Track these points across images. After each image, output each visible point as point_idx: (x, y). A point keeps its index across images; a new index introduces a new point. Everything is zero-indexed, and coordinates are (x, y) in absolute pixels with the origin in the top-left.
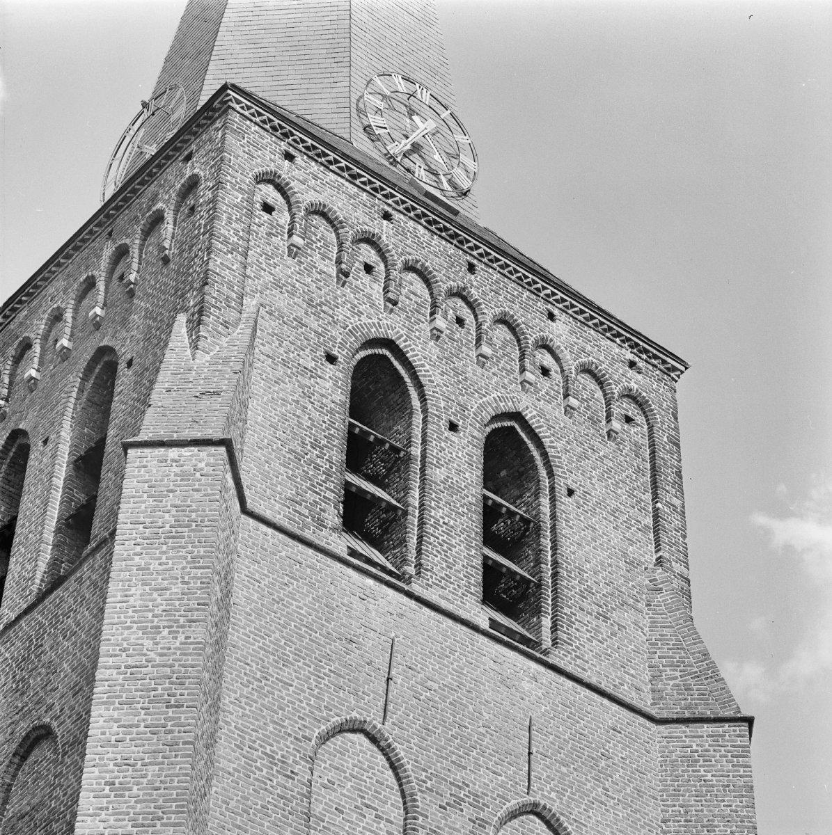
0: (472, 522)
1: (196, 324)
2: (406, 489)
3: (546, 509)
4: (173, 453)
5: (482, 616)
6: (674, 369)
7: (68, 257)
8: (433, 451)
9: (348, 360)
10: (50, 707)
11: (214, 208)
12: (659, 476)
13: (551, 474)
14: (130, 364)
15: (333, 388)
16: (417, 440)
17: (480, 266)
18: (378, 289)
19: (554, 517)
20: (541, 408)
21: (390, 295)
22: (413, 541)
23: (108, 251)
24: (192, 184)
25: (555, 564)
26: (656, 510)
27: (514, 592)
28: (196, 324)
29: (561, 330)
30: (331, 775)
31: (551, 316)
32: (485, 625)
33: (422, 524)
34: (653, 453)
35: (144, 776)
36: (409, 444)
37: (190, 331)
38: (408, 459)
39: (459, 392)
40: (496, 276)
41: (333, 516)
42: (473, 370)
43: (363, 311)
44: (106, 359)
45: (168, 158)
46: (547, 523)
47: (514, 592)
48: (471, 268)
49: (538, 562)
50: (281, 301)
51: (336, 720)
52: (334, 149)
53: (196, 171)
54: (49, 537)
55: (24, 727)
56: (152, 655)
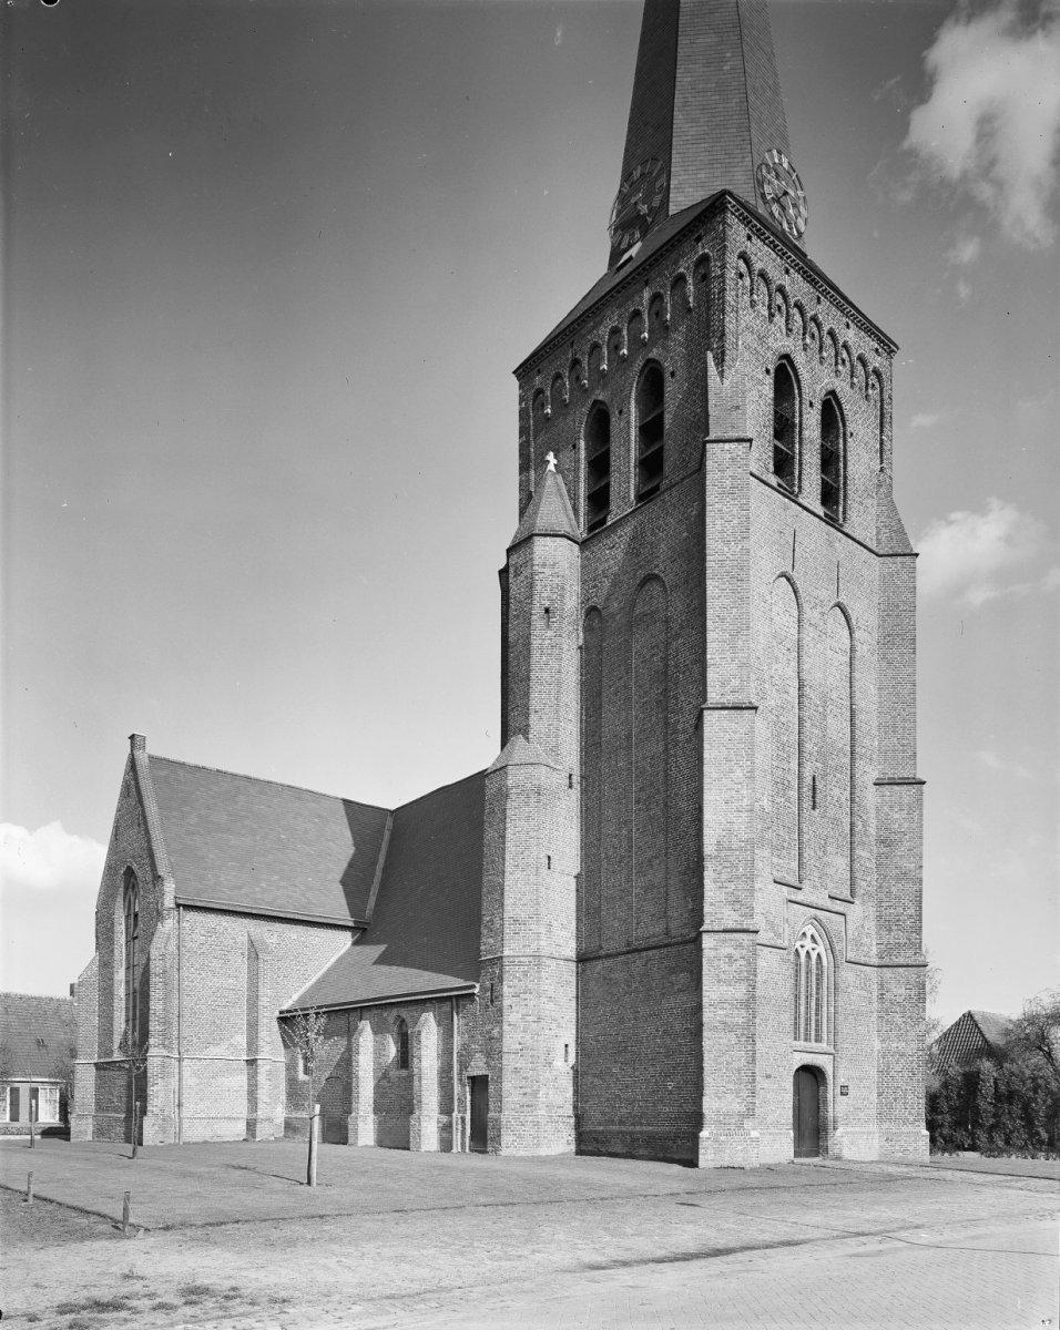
1: (720, 361)
2: (793, 443)
3: (841, 446)
4: (727, 446)
6: (893, 351)
7: (619, 292)
10: (657, 566)
11: (724, 282)
12: (883, 421)
13: (844, 425)
14: (673, 374)
16: (797, 414)
17: (754, 238)
18: (783, 320)
19: (845, 450)
20: (842, 387)
21: (790, 326)
22: (797, 473)
23: (647, 294)
24: (705, 259)
25: (845, 477)
26: (881, 440)
28: (720, 361)
29: (851, 335)
32: (822, 514)
33: (801, 464)
34: (882, 406)
36: (794, 417)
37: (717, 365)
38: (794, 425)
39: (815, 379)
42: (818, 366)
43: (782, 342)
44: (651, 365)
45: (685, 236)
46: (842, 453)
49: (838, 476)
52: (768, 229)
53: (706, 251)
54: (632, 469)
55: (641, 574)
56: (728, 555)
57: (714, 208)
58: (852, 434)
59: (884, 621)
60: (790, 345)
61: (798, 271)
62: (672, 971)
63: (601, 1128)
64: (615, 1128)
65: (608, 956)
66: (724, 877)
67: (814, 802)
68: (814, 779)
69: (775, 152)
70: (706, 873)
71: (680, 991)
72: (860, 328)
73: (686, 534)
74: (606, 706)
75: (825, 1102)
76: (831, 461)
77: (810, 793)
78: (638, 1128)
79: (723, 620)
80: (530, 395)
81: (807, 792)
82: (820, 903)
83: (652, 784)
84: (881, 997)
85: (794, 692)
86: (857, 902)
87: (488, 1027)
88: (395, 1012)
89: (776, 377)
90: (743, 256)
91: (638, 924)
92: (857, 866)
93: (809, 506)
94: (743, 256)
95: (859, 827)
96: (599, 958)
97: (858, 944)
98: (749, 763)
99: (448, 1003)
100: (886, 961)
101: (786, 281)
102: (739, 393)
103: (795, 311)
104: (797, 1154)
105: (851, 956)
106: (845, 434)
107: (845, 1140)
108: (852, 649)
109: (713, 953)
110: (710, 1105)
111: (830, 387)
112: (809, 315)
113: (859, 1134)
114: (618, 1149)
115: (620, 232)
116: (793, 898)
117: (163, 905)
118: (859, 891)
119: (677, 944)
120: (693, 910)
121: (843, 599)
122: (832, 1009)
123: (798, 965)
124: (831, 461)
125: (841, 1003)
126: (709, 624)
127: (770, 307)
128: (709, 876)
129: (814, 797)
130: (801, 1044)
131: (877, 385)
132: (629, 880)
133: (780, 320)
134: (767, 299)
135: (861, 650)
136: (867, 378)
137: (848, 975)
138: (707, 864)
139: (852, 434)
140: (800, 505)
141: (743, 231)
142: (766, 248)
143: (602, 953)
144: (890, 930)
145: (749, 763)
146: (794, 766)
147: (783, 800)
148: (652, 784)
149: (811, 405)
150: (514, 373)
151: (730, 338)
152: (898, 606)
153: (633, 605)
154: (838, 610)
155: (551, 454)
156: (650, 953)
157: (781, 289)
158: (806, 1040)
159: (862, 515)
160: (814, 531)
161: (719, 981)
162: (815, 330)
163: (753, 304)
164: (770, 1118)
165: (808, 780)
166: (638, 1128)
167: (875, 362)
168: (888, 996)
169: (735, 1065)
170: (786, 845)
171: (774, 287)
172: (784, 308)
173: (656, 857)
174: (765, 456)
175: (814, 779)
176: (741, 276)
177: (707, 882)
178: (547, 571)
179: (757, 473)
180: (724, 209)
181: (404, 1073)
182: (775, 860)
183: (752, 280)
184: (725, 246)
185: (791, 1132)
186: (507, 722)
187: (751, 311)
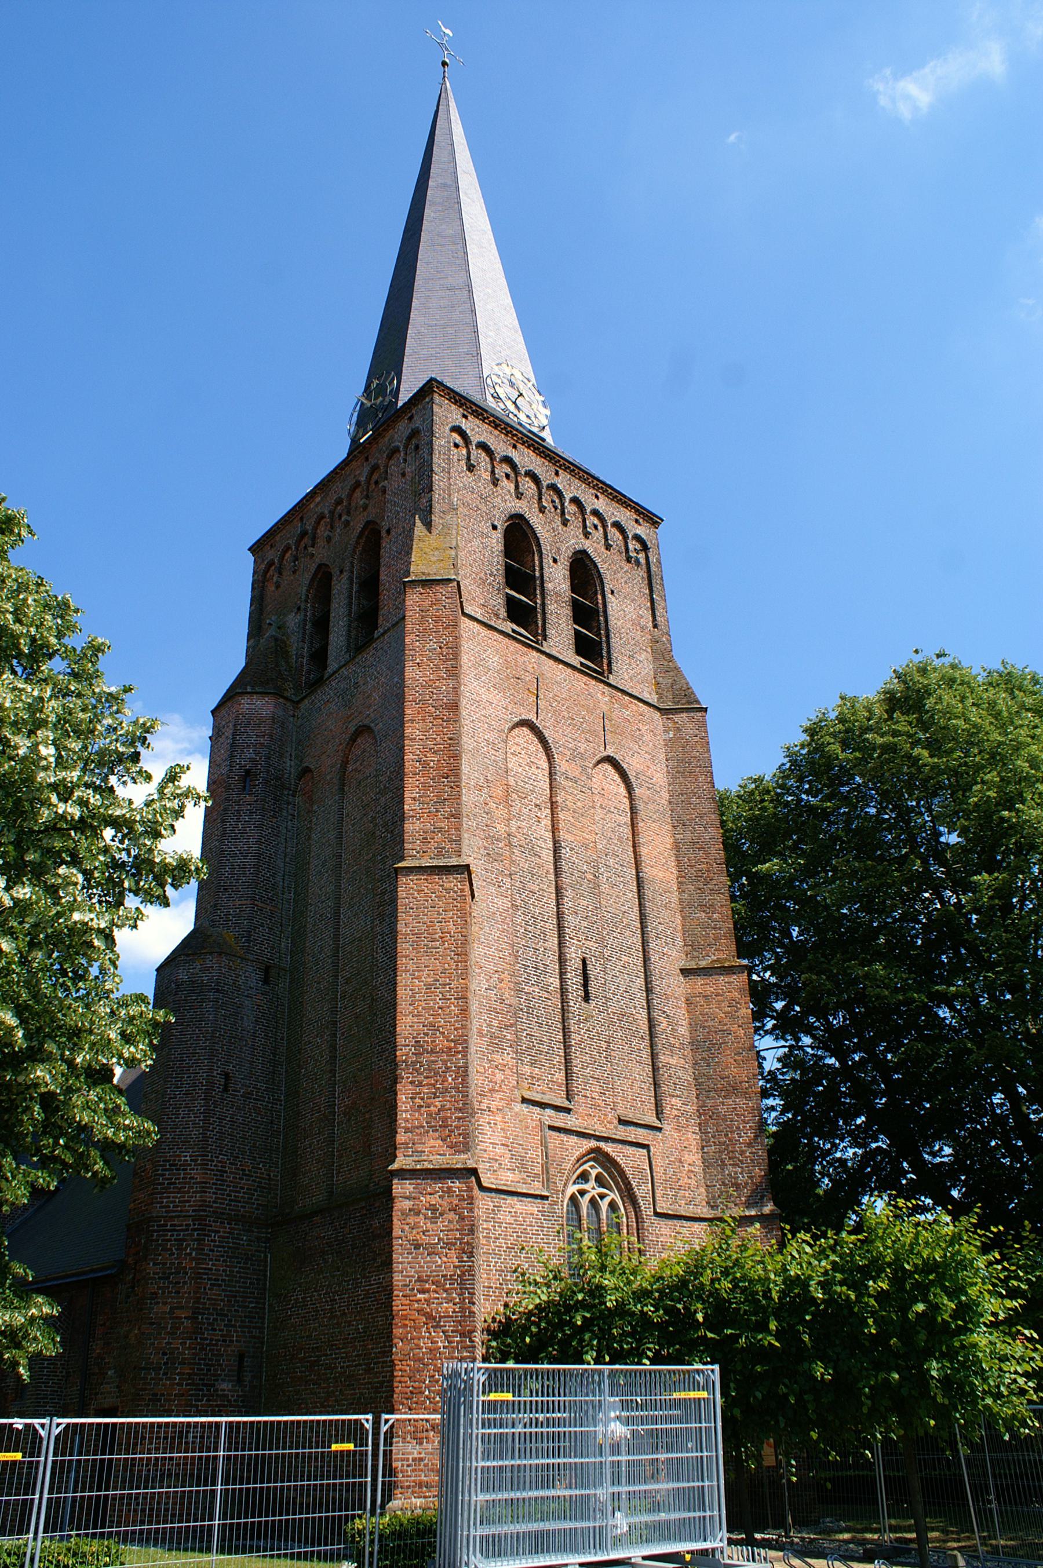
0: (567, 611)
5: (576, 660)
8: (546, 575)
9: (501, 526)
14: (388, 532)
15: (496, 541)
18: (513, 486)
20: (594, 547)
27: (593, 649)
29: (601, 504)
30: (515, 748)
31: (597, 497)
35: (426, 756)
36: (534, 571)
39: (557, 542)
40: (569, 476)
41: (503, 613)
43: (506, 502)
44: (371, 527)
47: (593, 649)
48: (557, 474)
49: (599, 629)
50: (468, 497)
51: (516, 720)
57: (429, 388)
61: (528, 447)
68: (584, 960)
77: (580, 979)
81: (574, 980)
82: (601, 1131)
85: (548, 856)
86: (665, 1126)
93: (557, 655)
95: (663, 1024)
134: (489, 466)
150: (249, 549)
154: (607, 767)
159: (633, 666)
160: (565, 682)
165: (574, 964)
175: (584, 960)
177: (402, 1098)
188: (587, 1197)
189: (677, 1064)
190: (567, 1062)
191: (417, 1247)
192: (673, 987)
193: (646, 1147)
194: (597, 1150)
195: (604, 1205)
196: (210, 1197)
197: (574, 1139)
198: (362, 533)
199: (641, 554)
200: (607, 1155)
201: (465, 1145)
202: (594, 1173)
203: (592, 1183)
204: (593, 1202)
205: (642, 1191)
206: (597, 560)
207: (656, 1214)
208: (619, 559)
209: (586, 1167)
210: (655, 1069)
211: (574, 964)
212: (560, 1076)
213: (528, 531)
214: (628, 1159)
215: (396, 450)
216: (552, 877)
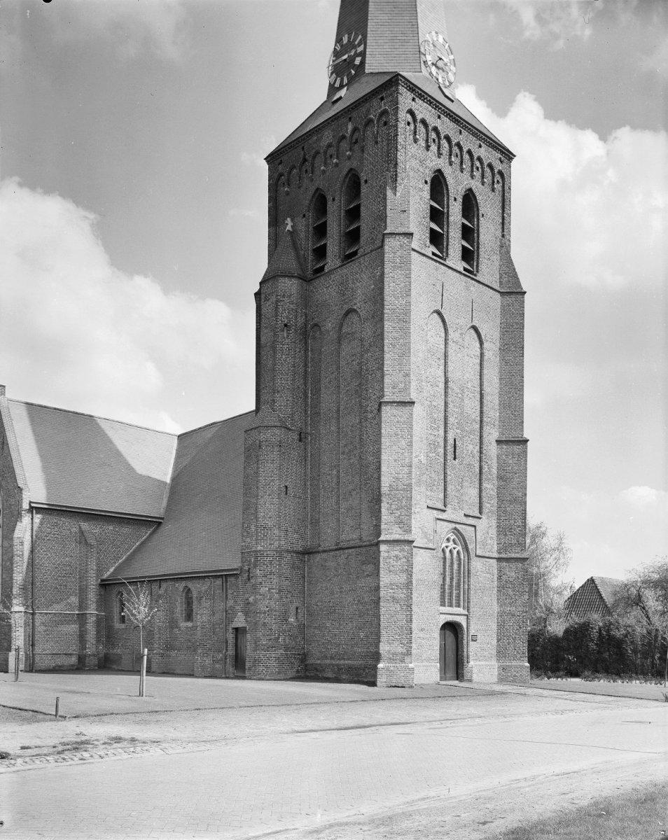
8: (451, 211)
14: (366, 181)
17: (417, 99)
20: (475, 185)
22: (445, 244)
25: (478, 243)
39: (457, 183)
49: (473, 242)
55: (346, 307)
58: (483, 215)
59: (504, 335)
60: (442, 163)
61: (446, 116)
62: (363, 563)
63: (319, 662)
64: (328, 662)
65: (324, 551)
66: (393, 507)
67: (455, 455)
68: (455, 440)
69: (433, 33)
70: (382, 504)
71: (368, 575)
72: (489, 146)
73: (373, 286)
74: (323, 390)
75: (462, 647)
76: (468, 233)
77: (453, 449)
78: (342, 662)
79: (394, 346)
80: (276, 175)
81: (450, 449)
83: (352, 443)
84: (500, 578)
85: (442, 385)
87: (247, 596)
88: (184, 584)
89: (431, 185)
90: (411, 112)
91: (343, 531)
92: (484, 494)
94: (411, 112)
95: (485, 469)
96: (319, 552)
97: (484, 544)
98: (409, 436)
99: (220, 579)
100: (503, 556)
101: (438, 123)
102: (408, 204)
103: (444, 141)
104: (441, 679)
105: (479, 552)
106: (478, 215)
107: (475, 670)
108: (482, 355)
109: (386, 554)
110: (384, 648)
111: (468, 187)
112: (454, 143)
113: (482, 663)
114: (330, 675)
115: (334, 75)
116: (440, 517)
117: (21, 507)
118: (485, 510)
119: (365, 546)
120: (376, 525)
121: (476, 323)
122: (466, 586)
123: (445, 558)
124: (468, 233)
125: (472, 581)
126: (386, 349)
127: (427, 141)
128: (384, 506)
129: (455, 452)
130: (443, 609)
131: (500, 181)
132: (338, 503)
133: (434, 148)
135: (487, 355)
136: (493, 178)
137: (477, 564)
138: (383, 499)
139: (483, 215)
140: (447, 266)
141: (410, 95)
142: (425, 104)
143: (320, 549)
144: (506, 535)
145: (409, 436)
146: (442, 432)
147: (434, 455)
148: (352, 443)
149: (455, 199)
150: (265, 159)
151: (400, 165)
152: (512, 326)
153: (341, 325)
154: (472, 331)
155: (289, 219)
156: (350, 551)
157: (435, 129)
158: (451, 606)
159: (489, 268)
160: (457, 285)
161: (390, 571)
162: (458, 151)
163: (416, 141)
164: (424, 656)
165: (451, 442)
166: (342, 662)
167: (498, 167)
168: (504, 577)
169: (400, 623)
170: (436, 483)
171: (430, 128)
172: (437, 140)
173: (354, 490)
174: (424, 237)
175: (455, 440)
176: (409, 124)
177: (383, 510)
178: (286, 300)
179: (417, 249)
180: (398, 84)
181: (190, 624)
182: (429, 493)
183: (416, 126)
184: (397, 107)
185: (438, 664)
186: (260, 338)
187: (415, 145)
188: (449, 549)
189: (490, 487)
190: (445, 490)
191: (390, 571)
192: (492, 450)
193: (475, 526)
194: (455, 529)
195: (455, 552)
196: (283, 543)
197: (446, 523)
198: (347, 175)
199: (500, 181)
200: (458, 530)
201: (409, 531)
202: (452, 538)
203: (452, 542)
204: (451, 551)
205: (471, 547)
206: (477, 194)
207: (476, 556)
208: (487, 189)
209: (449, 535)
210: (481, 491)
211: (451, 442)
212: (442, 496)
213: (442, 180)
214: (468, 532)
215: (371, 121)
216: (443, 397)
